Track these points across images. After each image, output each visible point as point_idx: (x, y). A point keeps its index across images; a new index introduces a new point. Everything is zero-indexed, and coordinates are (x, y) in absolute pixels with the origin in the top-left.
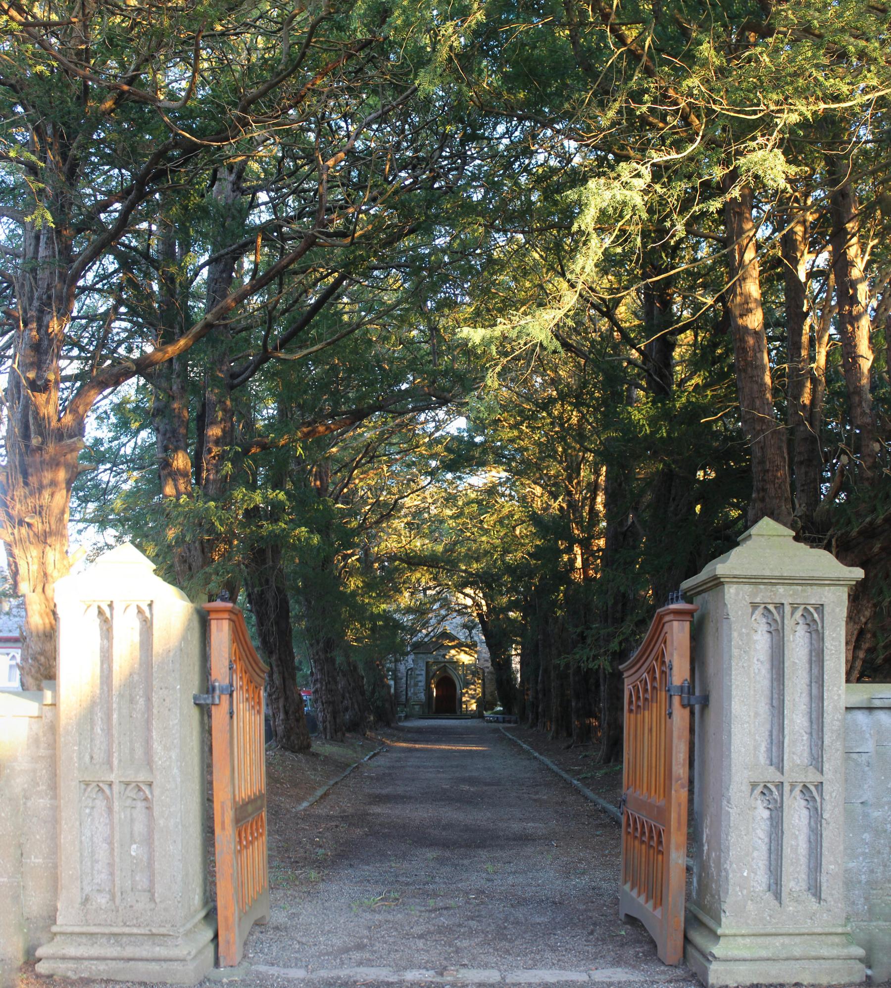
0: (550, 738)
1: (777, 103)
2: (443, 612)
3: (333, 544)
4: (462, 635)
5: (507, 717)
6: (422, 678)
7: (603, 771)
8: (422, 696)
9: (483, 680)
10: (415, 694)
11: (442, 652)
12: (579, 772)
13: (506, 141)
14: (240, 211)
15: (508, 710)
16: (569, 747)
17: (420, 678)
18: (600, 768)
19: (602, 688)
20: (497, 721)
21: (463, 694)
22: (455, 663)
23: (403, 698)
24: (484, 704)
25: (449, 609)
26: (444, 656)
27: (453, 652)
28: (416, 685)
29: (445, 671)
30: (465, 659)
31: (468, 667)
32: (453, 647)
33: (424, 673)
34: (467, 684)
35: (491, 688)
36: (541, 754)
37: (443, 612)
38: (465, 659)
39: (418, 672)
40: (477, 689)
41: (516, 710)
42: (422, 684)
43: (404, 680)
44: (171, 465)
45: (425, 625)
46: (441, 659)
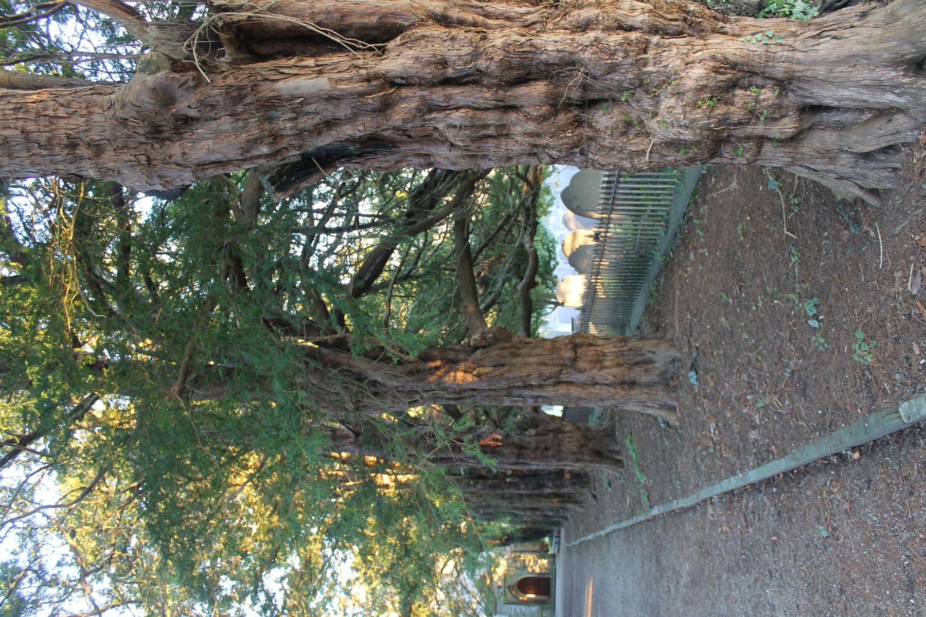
0: (581, 510)
2: (459, 588)
5: (555, 534)
6: (518, 608)
7: (638, 473)
8: (535, 609)
9: (521, 552)
12: (637, 502)
13: (826, 346)
15: (548, 533)
16: (595, 497)
18: (632, 476)
19: (534, 467)
20: (558, 543)
22: (505, 577)
24: (543, 552)
25: (456, 583)
27: (496, 578)
29: (513, 587)
30: (501, 570)
31: (509, 566)
32: (492, 579)
33: (513, 607)
34: (525, 567)
35: (528, 546)
36: (602, 528)
37: (459, 588)
38: (501, 570)
39: (513, 612)
40: (529, 558)
41: (549, 528)
42: (523, 608)
45: (469, 604)
46: (502, 590)
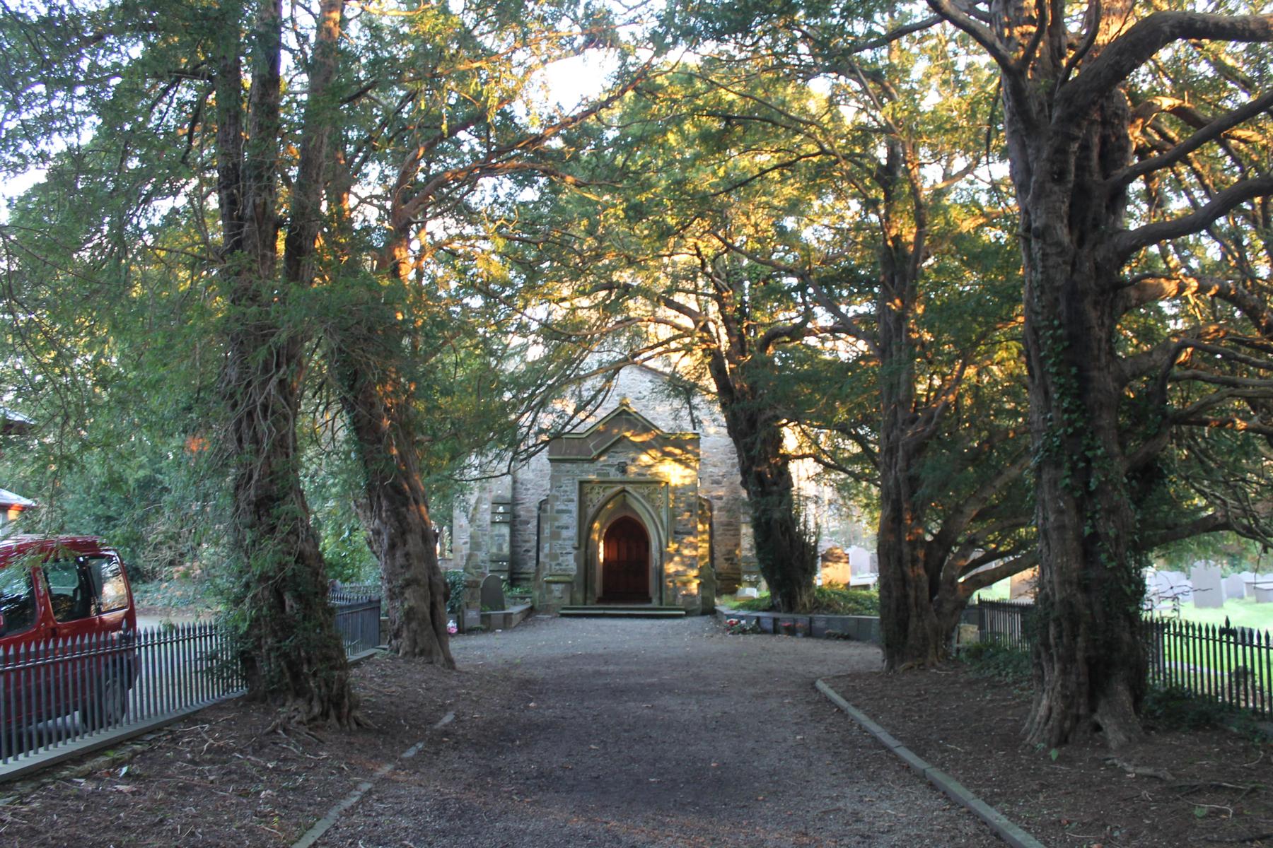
1: (89, 347)
3: (11, 70)
4: (663, 414)
5: (785, 618)
8: (570, 563)
10: (553, 557)
11: (621, 458)
14: (132, 580)
17: (565, 519)
20: (758, 629)
21: (666, 557)
22: (653, 484)
23: (531, 566)
26: (623, 469)
27: (645, 459)
28: (555, 535)
29: (625, 505)
30: (674, 473)
33: (574, 507)
38: (674, 473)
42: (571, 533)
43: (532, 526)
44: (1212, 80)
46: (614, 475)
